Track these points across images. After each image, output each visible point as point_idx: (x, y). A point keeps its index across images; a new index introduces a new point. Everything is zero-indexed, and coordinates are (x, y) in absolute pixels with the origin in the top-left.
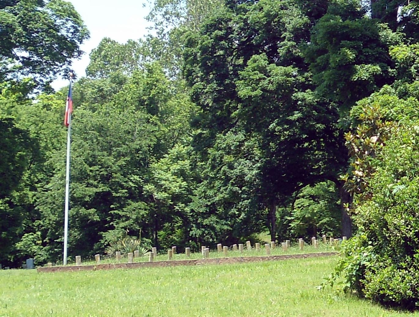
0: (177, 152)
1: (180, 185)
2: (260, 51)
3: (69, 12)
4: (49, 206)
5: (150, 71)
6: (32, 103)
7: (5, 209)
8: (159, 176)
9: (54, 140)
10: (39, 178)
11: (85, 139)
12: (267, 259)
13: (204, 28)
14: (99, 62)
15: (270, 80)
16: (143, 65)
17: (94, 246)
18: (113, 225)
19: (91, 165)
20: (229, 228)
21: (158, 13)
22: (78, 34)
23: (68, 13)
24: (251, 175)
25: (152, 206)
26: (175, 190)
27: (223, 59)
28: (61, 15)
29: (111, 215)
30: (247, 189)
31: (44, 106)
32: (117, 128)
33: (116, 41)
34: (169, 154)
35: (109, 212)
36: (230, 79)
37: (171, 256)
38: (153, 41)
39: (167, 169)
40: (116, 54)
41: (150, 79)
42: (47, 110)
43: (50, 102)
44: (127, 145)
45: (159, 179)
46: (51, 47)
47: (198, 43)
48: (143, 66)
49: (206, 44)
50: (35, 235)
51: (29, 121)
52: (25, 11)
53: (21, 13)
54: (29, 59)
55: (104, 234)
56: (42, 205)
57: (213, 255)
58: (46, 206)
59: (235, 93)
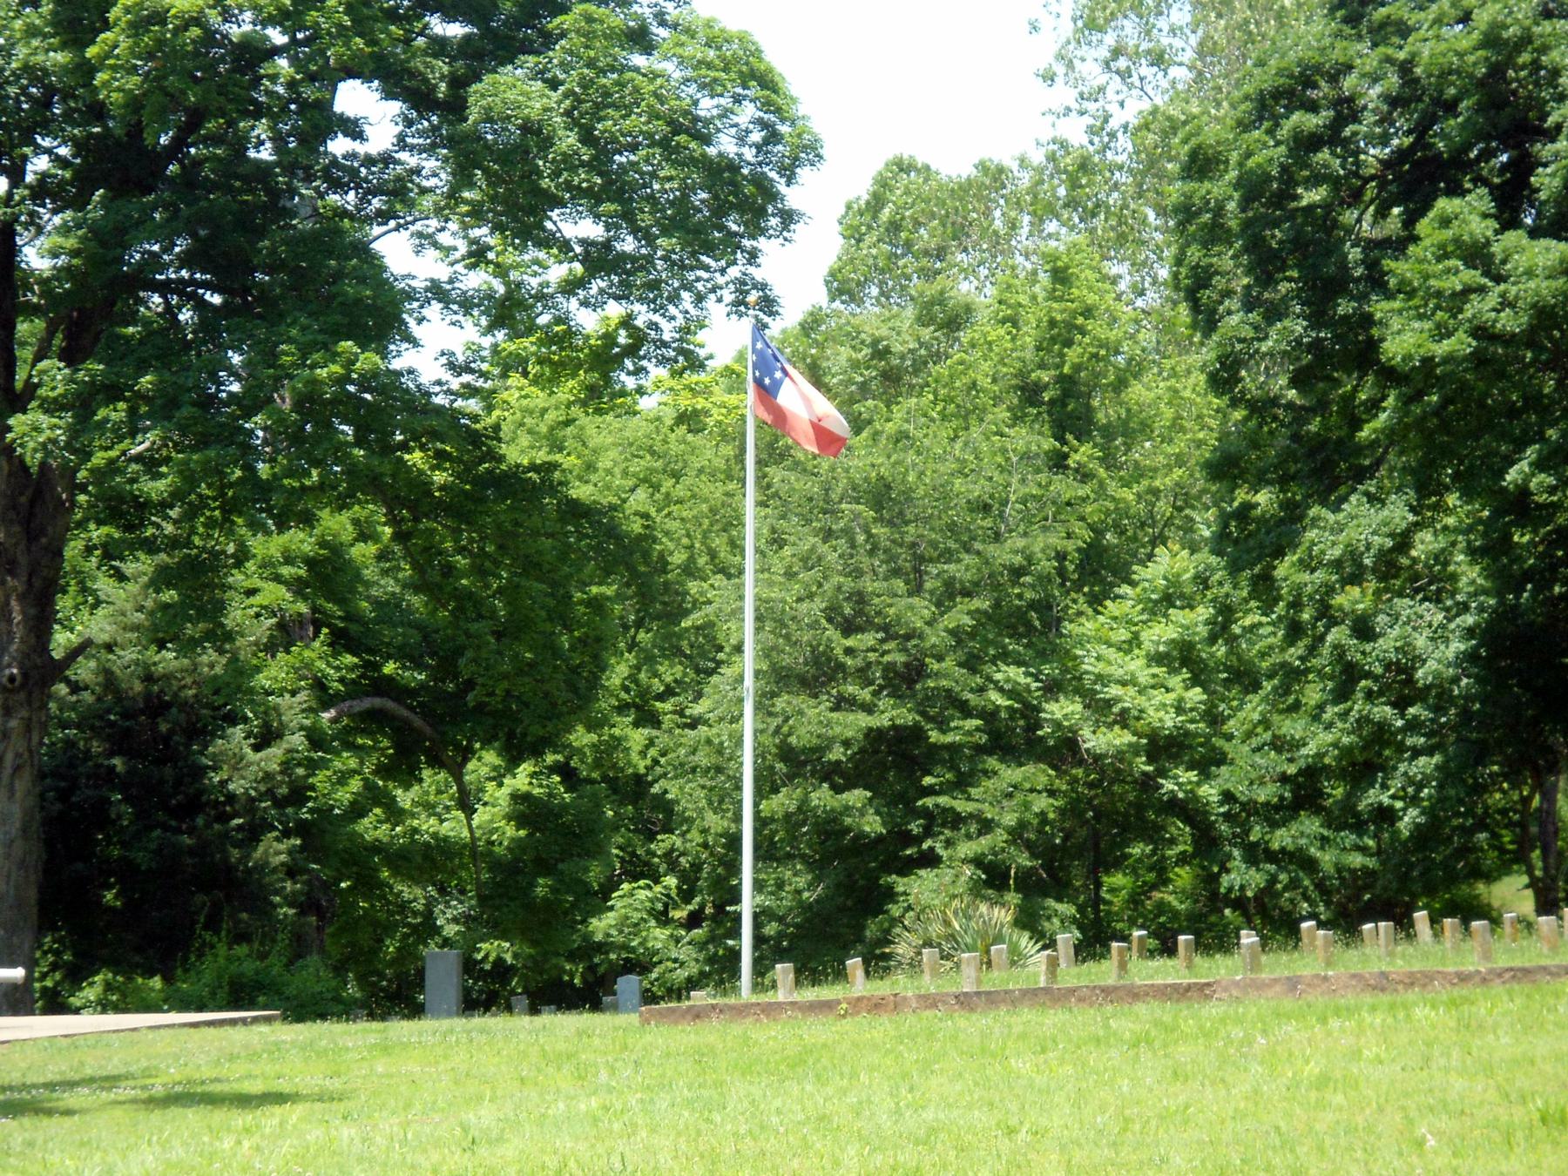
0: (1165, 578)
1: (1181, 700)
2: (1468, 186)
3: (744, 68)
4: (702, 781)
5: (1061, 276)
6: (638, 408)
7: (550, 795)
8: (1100, 668)
9: (717, 541)
10: (669, 679)
11: (828, 535)
12: (1477, 979)
13: (1247, 106)
14: (874, 249)
15: (1503, 295)
16: (1035, 253)
17: (863, 928)
18: (932, 849)
19: (849, 629)
20: (1371, 863)
21: (1084, 51)
22: (780, 147)
23: (741, 72)
24: (1439, 661)
25: (1075, 780)
26: (1161, 720)
27: (1323, 219)
28: (715, 80)
29: (927, 814)
30: (1425, 714)
31: (682, 418)
32: (944, 495)
33: (933, 168)
34: (1133, 584)
35: (920, 803)
36: (1353, 298)
37: (1123, 966)
38: (1068, 160)
39: (1130, 642)
40: (933, 216)
41: (1063, 305)
42: (690, 431)
43: (700, 403)
44: (978, 553)
45: (1100, 678)
46: (682, 203)
47: (1227, 162)
48: (1034, 259)
49: (1259, 165)
50: (658, 889)
51: (625, 473)
52: (586, 71)
53: (571, 82)
54: (607, 245)
55: (900, 884)
56: (676, 777)
57: (1280, 964)
58: (690, 781)
59: (1373, 345)
